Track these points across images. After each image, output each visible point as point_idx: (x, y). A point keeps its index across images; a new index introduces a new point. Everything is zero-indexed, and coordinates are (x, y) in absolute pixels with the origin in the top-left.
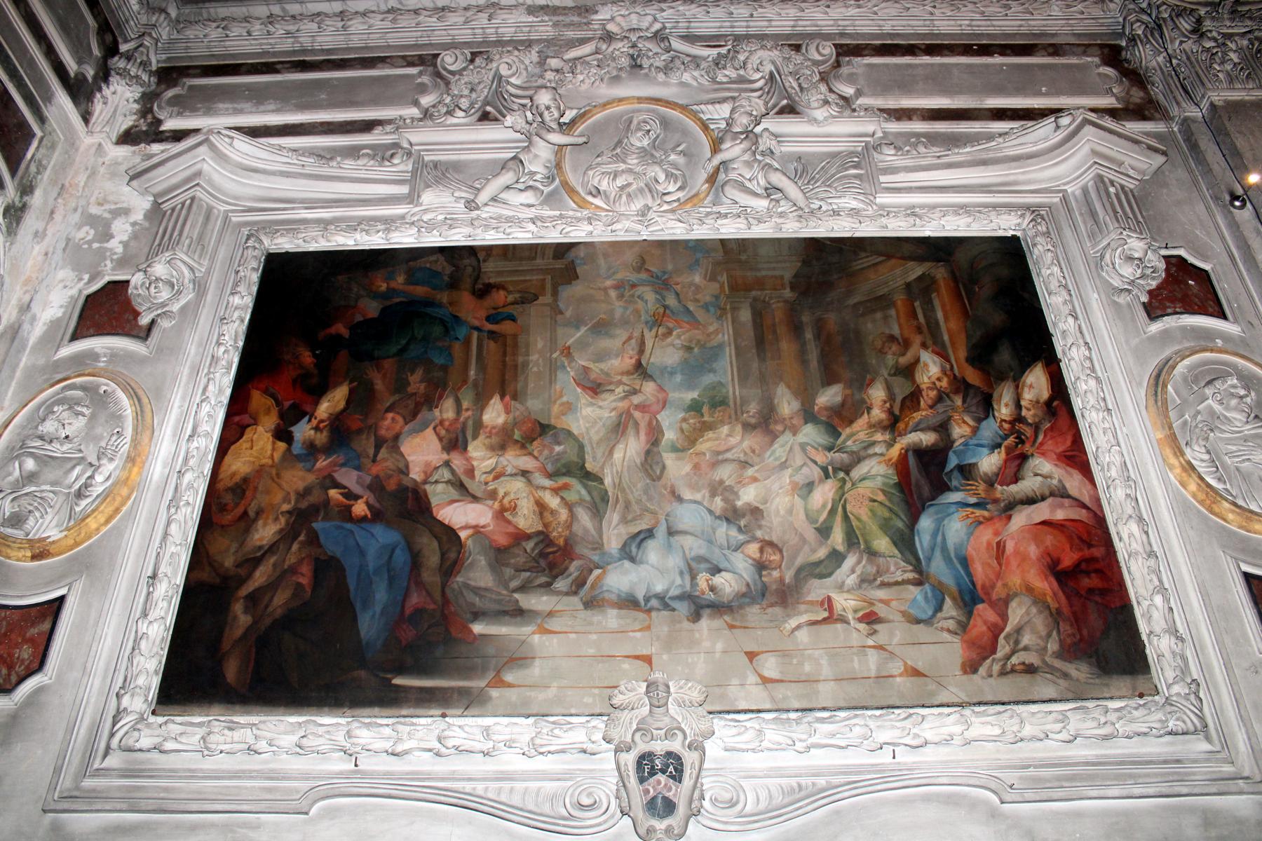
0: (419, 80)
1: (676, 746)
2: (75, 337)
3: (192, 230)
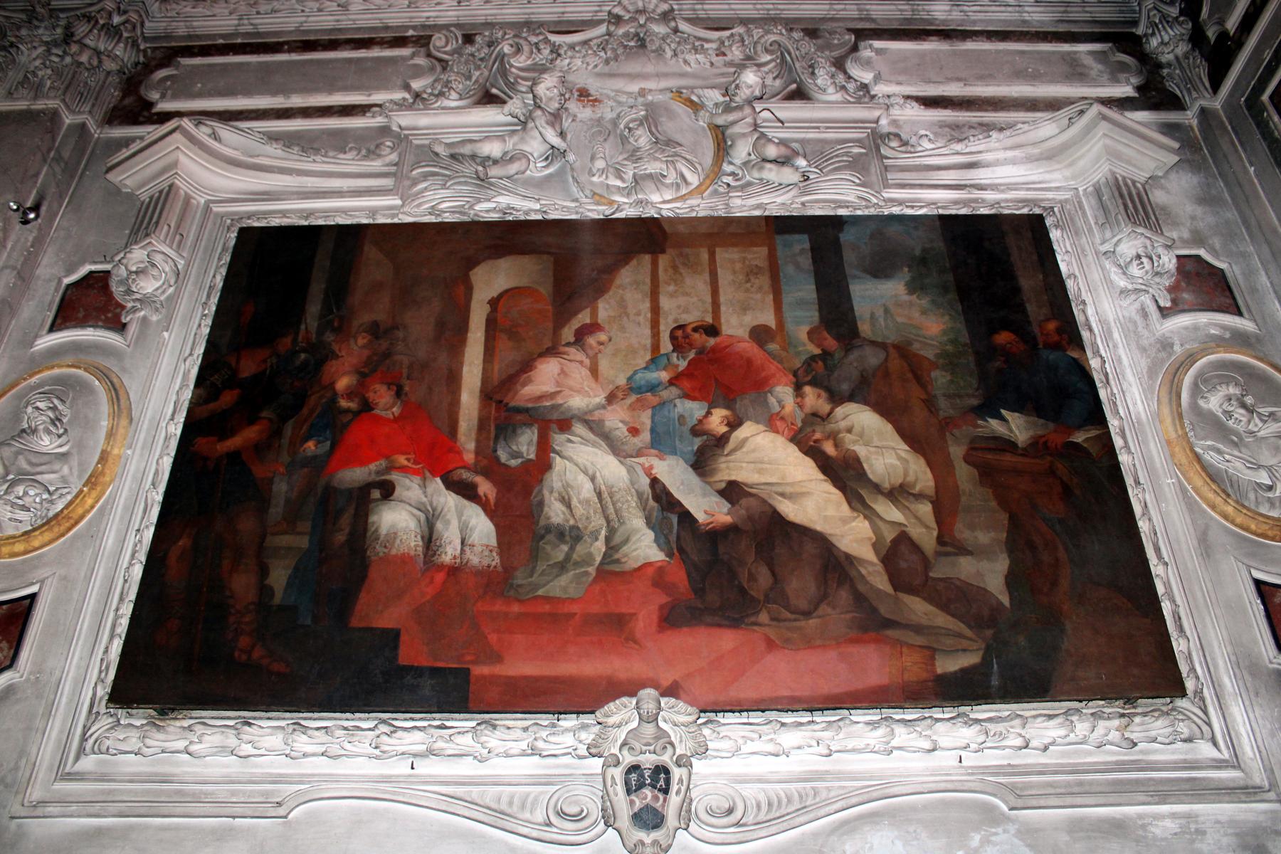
0: (412, 62)
1: (666, 758)
2: (52, 329)
3: (172, 218)
